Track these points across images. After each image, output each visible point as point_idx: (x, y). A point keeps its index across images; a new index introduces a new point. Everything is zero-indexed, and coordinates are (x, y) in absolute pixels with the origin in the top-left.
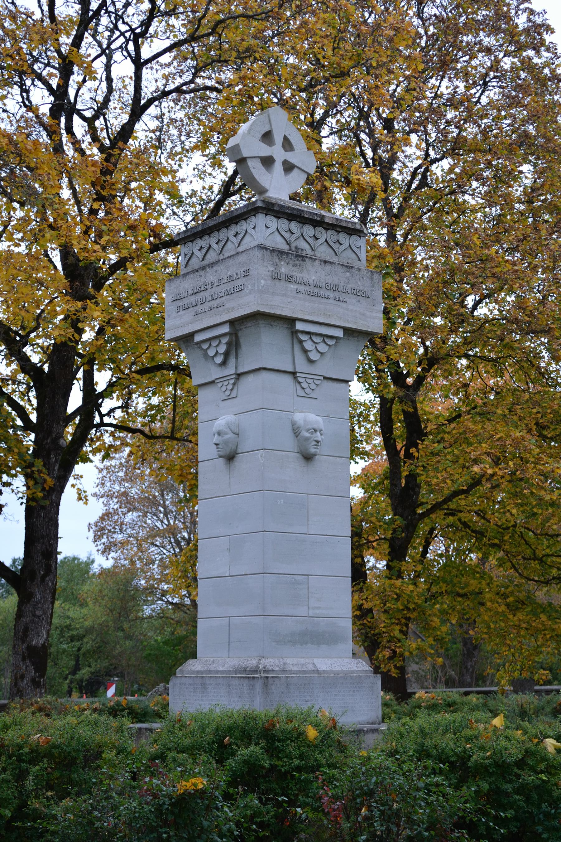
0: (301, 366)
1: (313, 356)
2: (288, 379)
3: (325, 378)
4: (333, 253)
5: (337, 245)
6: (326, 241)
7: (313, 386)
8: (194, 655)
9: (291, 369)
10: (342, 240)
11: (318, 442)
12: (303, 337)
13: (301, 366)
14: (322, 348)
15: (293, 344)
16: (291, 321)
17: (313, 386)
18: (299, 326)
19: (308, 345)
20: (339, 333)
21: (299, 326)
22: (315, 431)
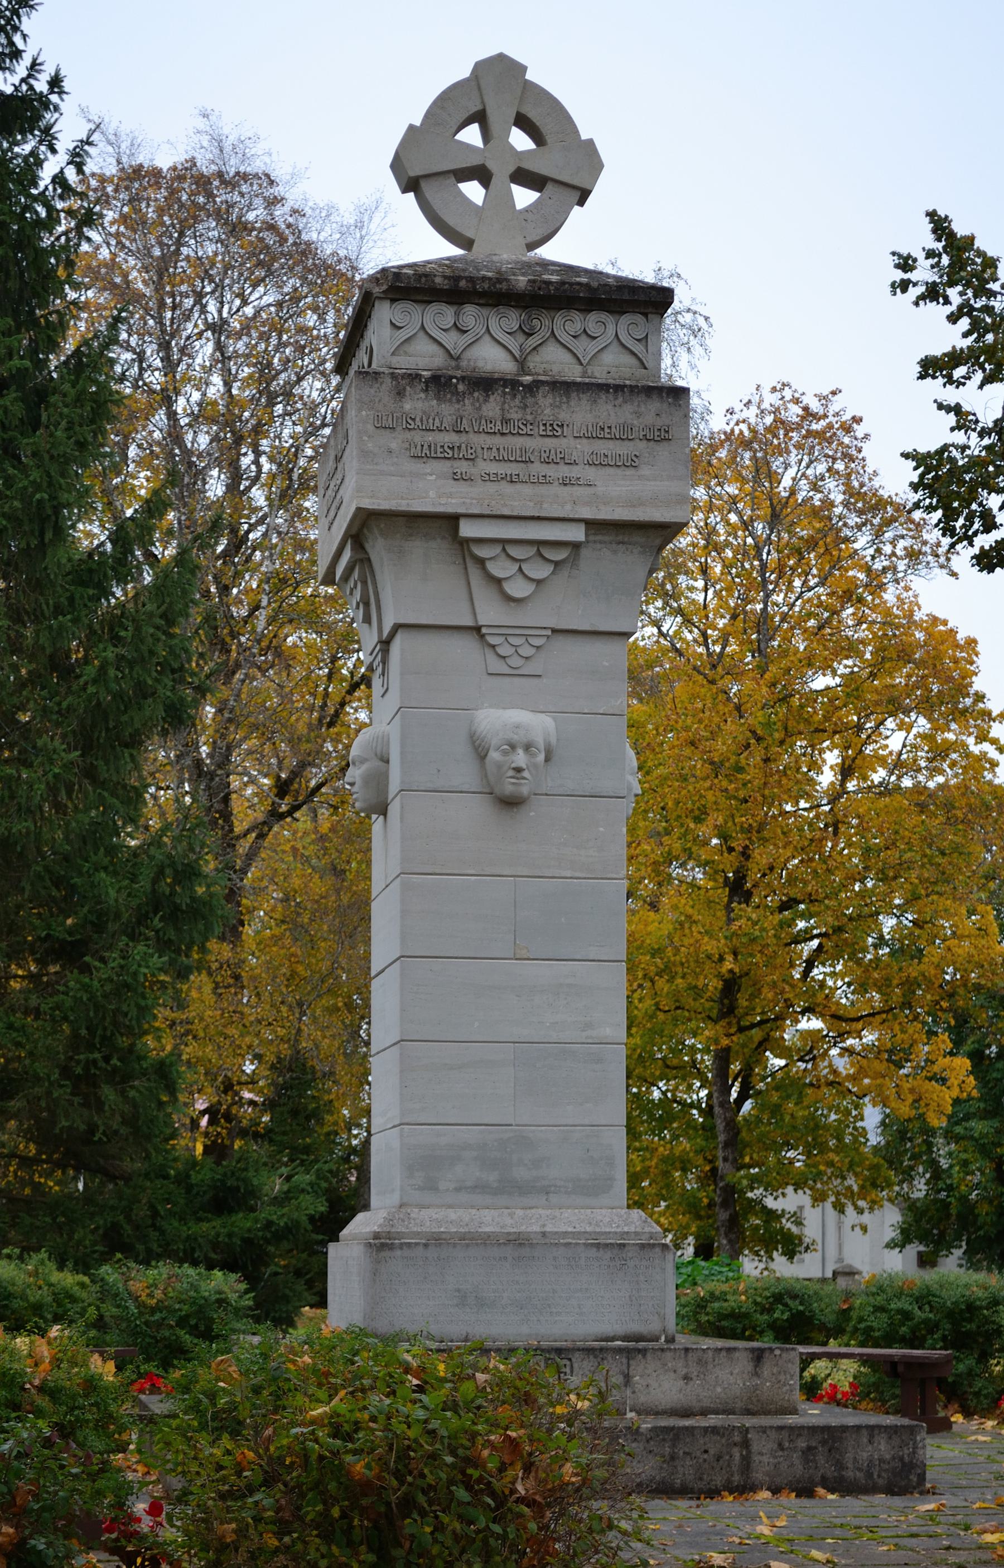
0: (490, 612)
1: (518, 588)
2: (465, 647)
3: (554, 631)
4: (574, 361)
5: (454, 335)
6: (423, 327)
7: (527, 651)
8: (366, 1207)
9: (470, 623)
10: (593, 329)
11: (519, 770)
12: (482, 552)
13: (490, 612)
14: (540, 571)
15: (466, 568)
16: (453, 520)
17: (527, 651)
18: (467, 530)
19: (499, 569)
20: (577, 534)
21: (467, 530)
22: (513, 747)
